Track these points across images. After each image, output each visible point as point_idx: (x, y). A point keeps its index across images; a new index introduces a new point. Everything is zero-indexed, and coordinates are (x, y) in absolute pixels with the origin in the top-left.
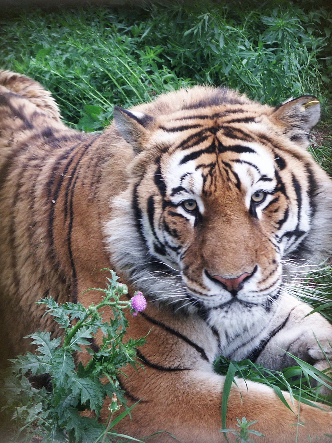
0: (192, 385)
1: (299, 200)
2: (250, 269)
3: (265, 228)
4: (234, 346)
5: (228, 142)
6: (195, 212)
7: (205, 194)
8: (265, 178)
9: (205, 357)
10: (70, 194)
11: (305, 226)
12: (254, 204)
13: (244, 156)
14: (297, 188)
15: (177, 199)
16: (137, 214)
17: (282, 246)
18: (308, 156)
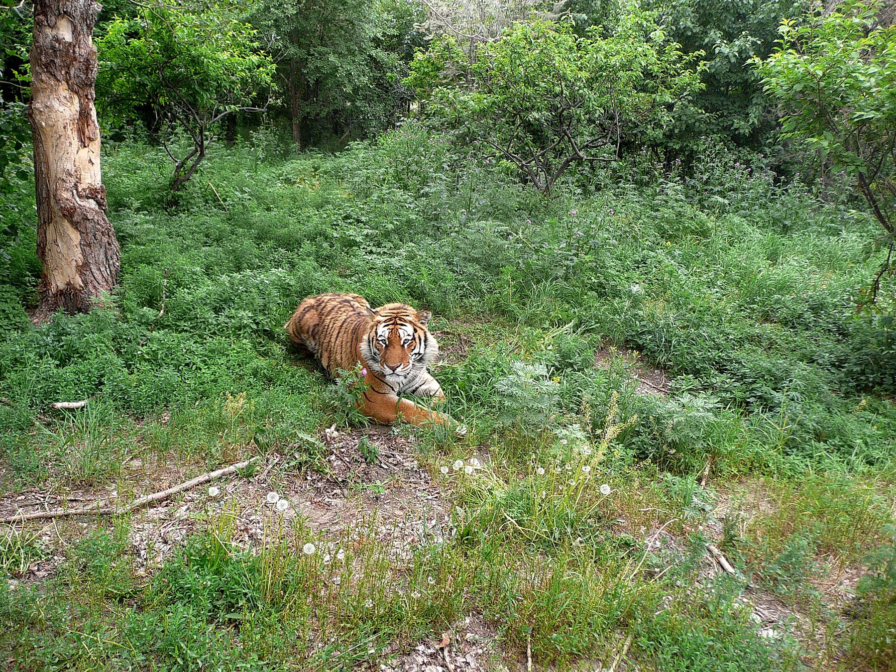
0: (389, 398)
1: (420, 343)
2: (399, 364)
3: (406, 351)
4: (406, 387)
5: (399, 322)
6: (385, 343)
7: (388, 338)
8: (409, 335)
9: (393, 390)
10: (357, 334)
11: (422, 352)
12: (404, 343)
13: (403, 327)
14: (420, 339)
15: (380, 339)
16: (369, 342)
17: (413, 357)
18: (426, 330)
